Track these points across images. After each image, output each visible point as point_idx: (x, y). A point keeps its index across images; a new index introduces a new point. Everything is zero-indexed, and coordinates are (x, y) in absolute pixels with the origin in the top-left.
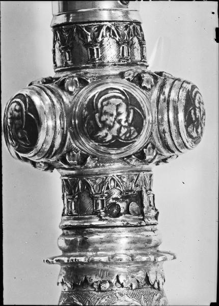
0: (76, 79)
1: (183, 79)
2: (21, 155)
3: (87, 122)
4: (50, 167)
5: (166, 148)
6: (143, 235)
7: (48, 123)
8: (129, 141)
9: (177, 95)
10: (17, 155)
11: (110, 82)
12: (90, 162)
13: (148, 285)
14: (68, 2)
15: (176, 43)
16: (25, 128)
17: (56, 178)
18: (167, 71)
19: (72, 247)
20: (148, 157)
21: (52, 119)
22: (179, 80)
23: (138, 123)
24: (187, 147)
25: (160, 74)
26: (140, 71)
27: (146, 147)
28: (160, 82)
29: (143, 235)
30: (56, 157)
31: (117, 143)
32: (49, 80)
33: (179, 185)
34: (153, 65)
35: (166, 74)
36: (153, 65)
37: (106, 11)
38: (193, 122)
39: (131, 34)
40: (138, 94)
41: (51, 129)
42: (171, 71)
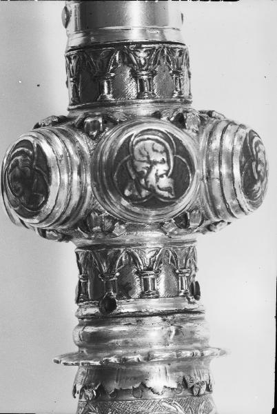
0: (100, 120)
1: (239, 122)
2: (26, 221)
3: (117, 173)
4: (66, 237)
5: (211, 215)
6: (113, 139)
7: (58, 178)
8: (170, 203)
9: (231, 143)
10: (22, 222)
11: (145, 131)
12: (119, 230)
13: (190, 389)
14: (87, 3)
15: (228, 72)
16: (28, 182)
17: (69, 250)
18: (218, 109)
19: (94, 343)
20: (192, 225)
21: (68, 173)
22: (232, 123)
23: (180, 187)
24: (242, 210)
25: (210, 113)
26: (181, 111)
27: (191, 212)
28: (209, 127)
29: (113, 139)
30: (76, 223)
31: (154, 201)
32: (62, 120)
33: (234, 270)
34: (198, 104)
35: (187, 208)
36: (198, 104)
37: (135, 23)
38: (250, 182)
39: (169, 57)
40: (179, 134)
41: (66, 186)
42: (224, 110)
